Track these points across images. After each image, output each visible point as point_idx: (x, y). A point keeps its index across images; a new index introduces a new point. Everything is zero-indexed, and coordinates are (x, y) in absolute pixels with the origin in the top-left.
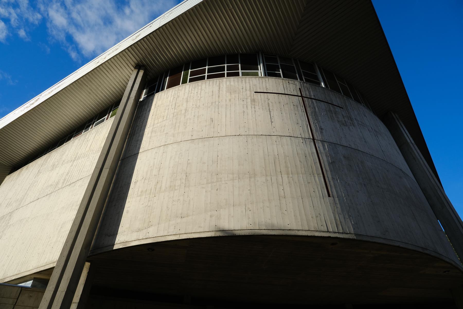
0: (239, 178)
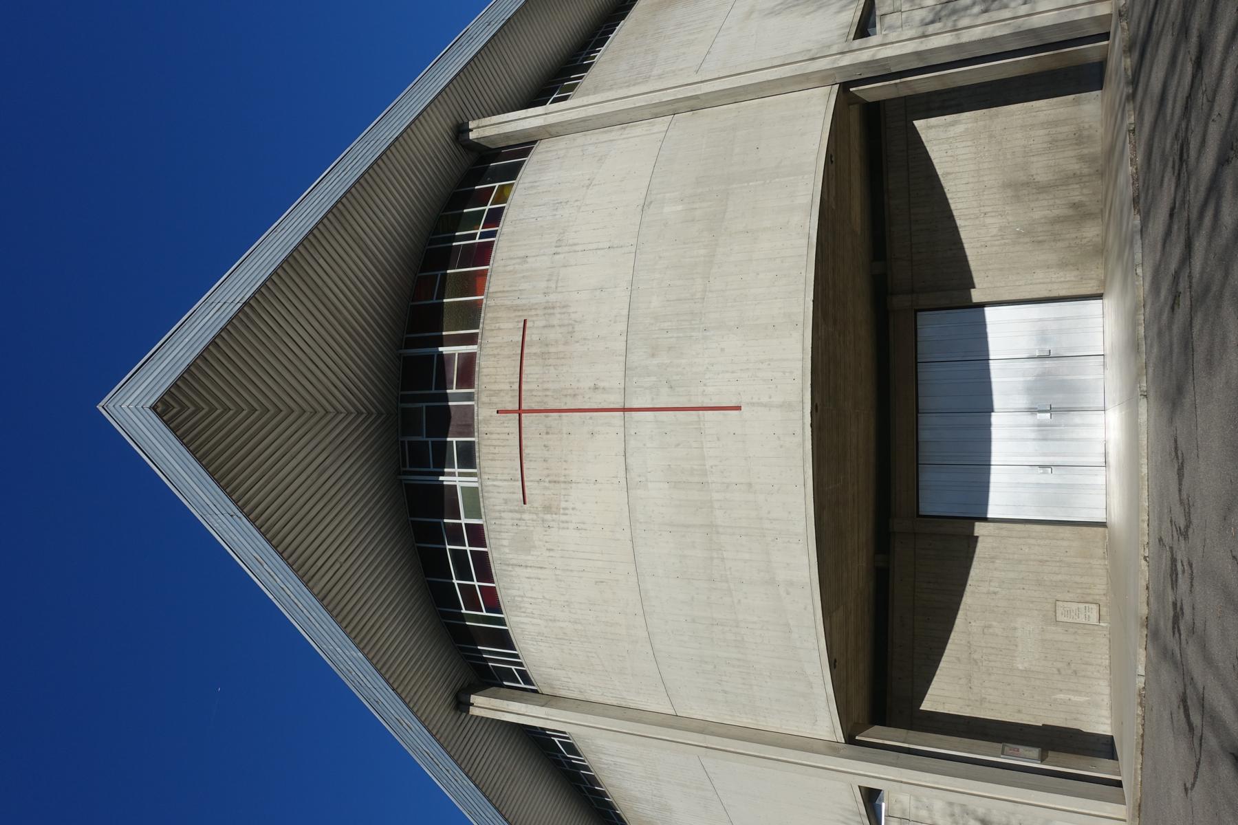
0: (720, 550)
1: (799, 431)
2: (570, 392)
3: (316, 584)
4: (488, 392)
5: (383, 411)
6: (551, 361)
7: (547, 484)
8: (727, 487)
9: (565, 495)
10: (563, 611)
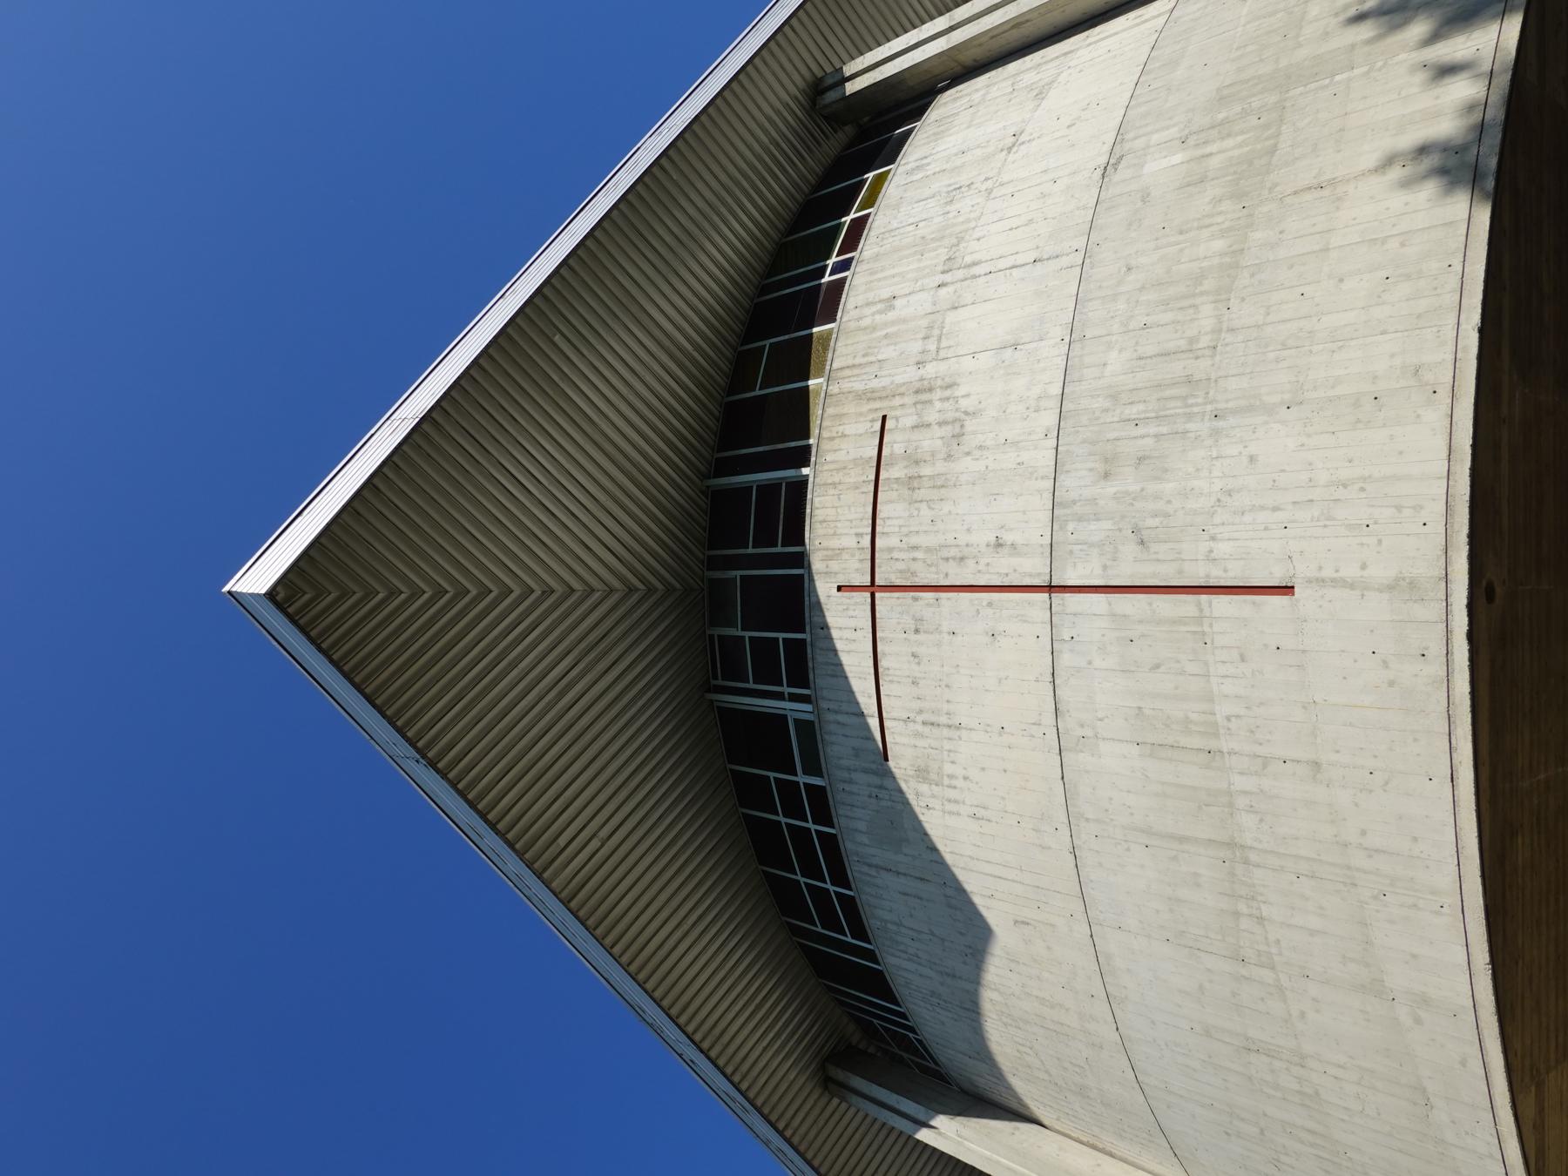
0: (1253, 898)
1: (1436, 648)
2: (953, 552)
3: (556, 874)
4: (825, 553)
5: (678, 586)
6: (922, 494)
7: (920, 728)
8: (1265, 766)
9: (950, 751)
10: (965, 963)
